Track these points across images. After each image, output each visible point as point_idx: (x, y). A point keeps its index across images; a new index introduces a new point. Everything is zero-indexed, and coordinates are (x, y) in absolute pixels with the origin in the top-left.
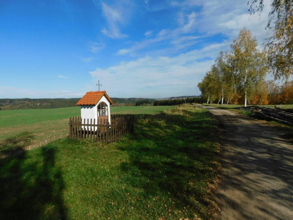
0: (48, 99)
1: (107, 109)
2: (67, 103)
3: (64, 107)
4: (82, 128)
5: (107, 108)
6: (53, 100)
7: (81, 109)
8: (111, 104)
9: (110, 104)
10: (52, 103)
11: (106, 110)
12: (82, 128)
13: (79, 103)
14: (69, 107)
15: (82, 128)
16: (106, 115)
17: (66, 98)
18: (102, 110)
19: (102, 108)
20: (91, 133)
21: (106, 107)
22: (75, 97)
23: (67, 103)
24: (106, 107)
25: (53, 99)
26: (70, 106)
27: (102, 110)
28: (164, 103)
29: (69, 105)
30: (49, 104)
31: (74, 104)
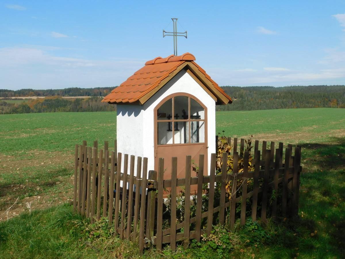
0: (233, 87)
1: (206, 121)
2: (276, 98)
3: (270, 108)
4: (260, 151)
5: (202, 117)
6: (245, 91)
7: (117, 116)
8: (219, 102)
9: (217, 104)
10: (241, 96)
11: (201, 123)
12: (260, 151)
13: (111, 97)
14: (282, 107)
15: (259, 150)
16: (202, 140)
17: (276, 86)
18: (191, 123)
19: (192, 117)
20: (130, 180)
21: (201, 114)
22: (297, 84)
23: (276, 98)
24: (201, 114)
25: (244, 88)
26: (284, 106)
27: (192, 124)
28: (95, 153)
29: (283, 103)
30: (235, 99)
31: (293, 102)
